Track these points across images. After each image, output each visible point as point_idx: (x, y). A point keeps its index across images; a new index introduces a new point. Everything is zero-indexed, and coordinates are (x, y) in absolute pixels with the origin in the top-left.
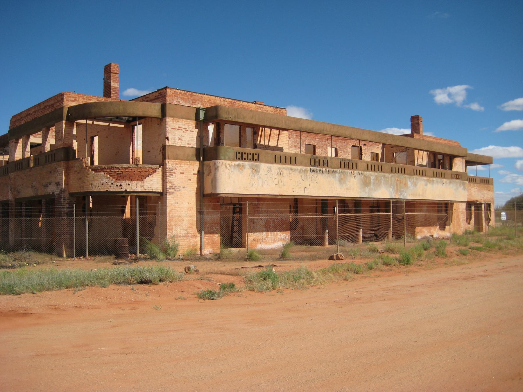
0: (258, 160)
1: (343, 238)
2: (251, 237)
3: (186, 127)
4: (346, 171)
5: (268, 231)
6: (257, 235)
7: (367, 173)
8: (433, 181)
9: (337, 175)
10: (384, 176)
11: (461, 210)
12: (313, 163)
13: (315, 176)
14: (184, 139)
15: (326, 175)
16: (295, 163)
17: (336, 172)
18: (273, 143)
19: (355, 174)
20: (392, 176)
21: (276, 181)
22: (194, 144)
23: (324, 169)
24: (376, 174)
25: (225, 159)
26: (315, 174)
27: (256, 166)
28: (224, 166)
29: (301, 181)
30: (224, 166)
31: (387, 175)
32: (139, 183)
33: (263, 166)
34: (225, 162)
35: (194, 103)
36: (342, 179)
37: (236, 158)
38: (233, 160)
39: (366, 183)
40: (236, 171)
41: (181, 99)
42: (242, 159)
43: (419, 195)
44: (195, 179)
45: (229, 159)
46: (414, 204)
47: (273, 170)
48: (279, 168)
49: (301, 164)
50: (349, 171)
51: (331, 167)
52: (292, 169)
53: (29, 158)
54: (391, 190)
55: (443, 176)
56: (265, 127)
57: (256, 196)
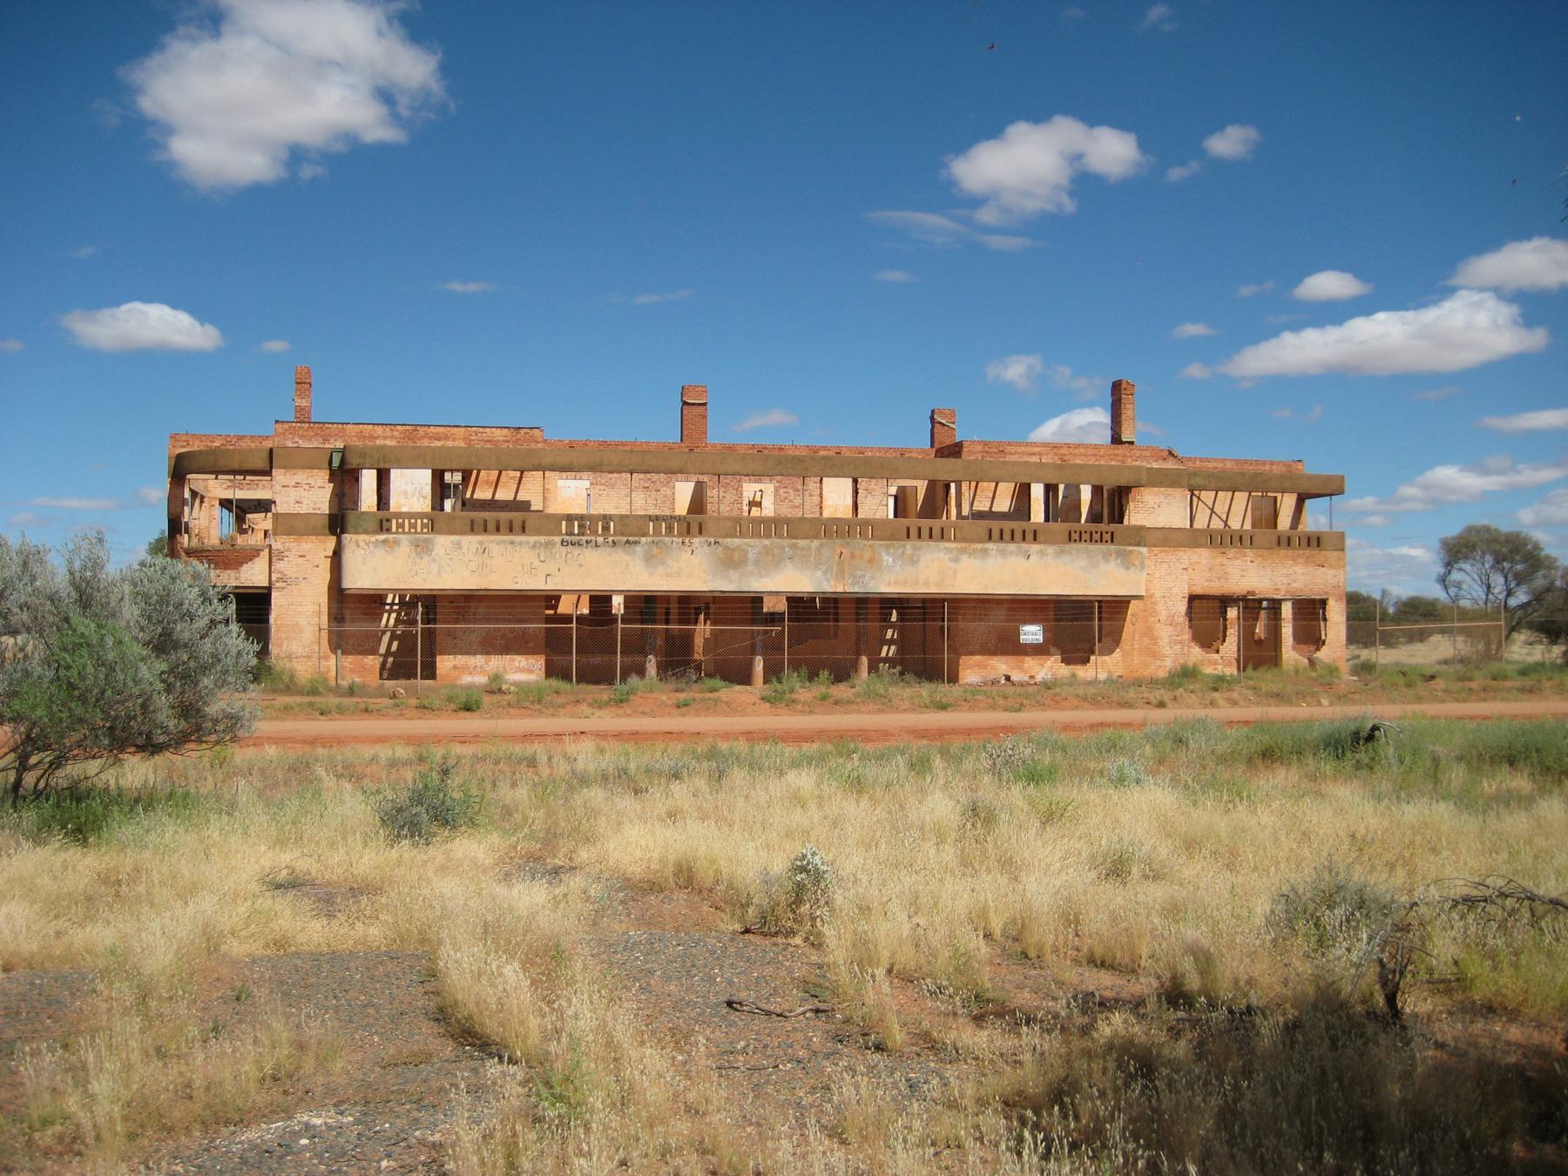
1: (795, 666)
2: (445, 663)
3: (311, 481)
5: (488, 653)
6: (461, 660)
9: (638, 549)
11: (1163, 616)
14: (305, 501)
18: (504, 494)
21: (472, 566)
22: (325, 509)
25: (357, 533)
26: (576, 551)
27: (426, 541)
28: (353, 545)
29: (536, 562)
30: (353, 545)
32: (232, 573)
34: (355, 537)
35: (326, 440)
38: (376, 533)
40: (380, 552)
41: (302, 437)
43: (927, 583)
44: (326, 565)
45: (366, 532)
47: (465, 547)
48: (481, 543)
52: (512, 543)
53: (1533, 305)
54: (819, 573)
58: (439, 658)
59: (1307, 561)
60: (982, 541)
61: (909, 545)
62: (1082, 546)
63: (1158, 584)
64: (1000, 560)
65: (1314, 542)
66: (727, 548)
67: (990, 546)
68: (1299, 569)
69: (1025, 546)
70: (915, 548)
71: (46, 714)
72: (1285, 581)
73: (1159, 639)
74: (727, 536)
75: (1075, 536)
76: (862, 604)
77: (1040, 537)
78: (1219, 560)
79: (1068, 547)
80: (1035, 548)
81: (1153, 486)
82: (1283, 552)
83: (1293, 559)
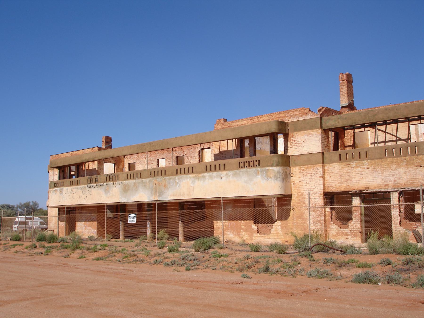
0: (259, 165)
4: (110, 183)
7: (126, 182)
8: (204, 176)
10: (142, 181)
12: (89, 182)
13: (90, 190)
15: (96, 189)
16: (165, 175)
17: (103, 185)
19: (117, 184)
20: (150, 181)
23: (95, 185)
24: (134, 181)
29: (82, 195)
31: (144, 180)
33: (65, 189)
36: (107, 190)
37: (239, 167)
39: (126, 190)
42: (254, 166)
43: (184, 195)
46: (212, 204)
49: (83, 184)
50: (112, 183)
51: (100, 183)
55: (97, 181)
56: (86, 162)
57: (234, 198)
58: (76, 222)
59: (408, 164)
60: (203, 172)
61: (177, 177)
62: (245, 169)
63: (309, 186)
64: (210, 181)
65: (191, 170)
66: (124, 184)
67: (206, 174)
68: (402, 170)
69: (220, 173)
70: (179, 179)
71: (0, 240)
72: (392, 179)
73: (309, 216)
74: (125, 180)
75: (242, 165)
76: (164, 206)
77: (227, 167)
78: (346, 169)
79: (238, 171)
80: (224, 173)
81: (301, 130)
82: (389, 160)
83: (398, 164)
